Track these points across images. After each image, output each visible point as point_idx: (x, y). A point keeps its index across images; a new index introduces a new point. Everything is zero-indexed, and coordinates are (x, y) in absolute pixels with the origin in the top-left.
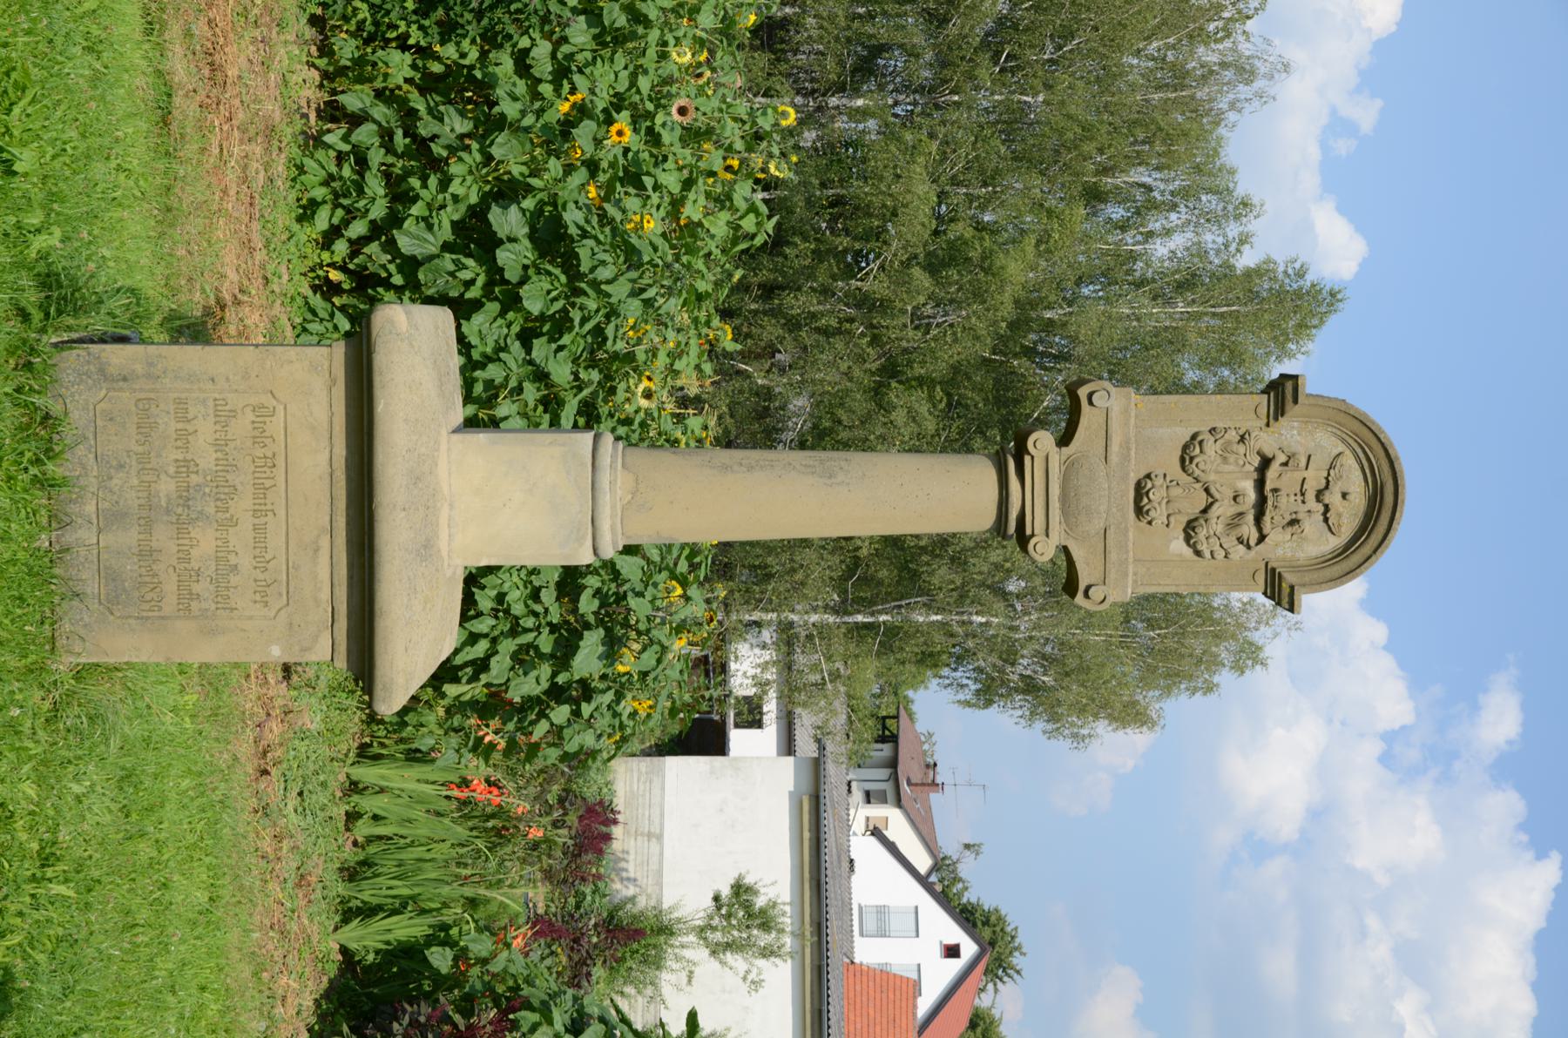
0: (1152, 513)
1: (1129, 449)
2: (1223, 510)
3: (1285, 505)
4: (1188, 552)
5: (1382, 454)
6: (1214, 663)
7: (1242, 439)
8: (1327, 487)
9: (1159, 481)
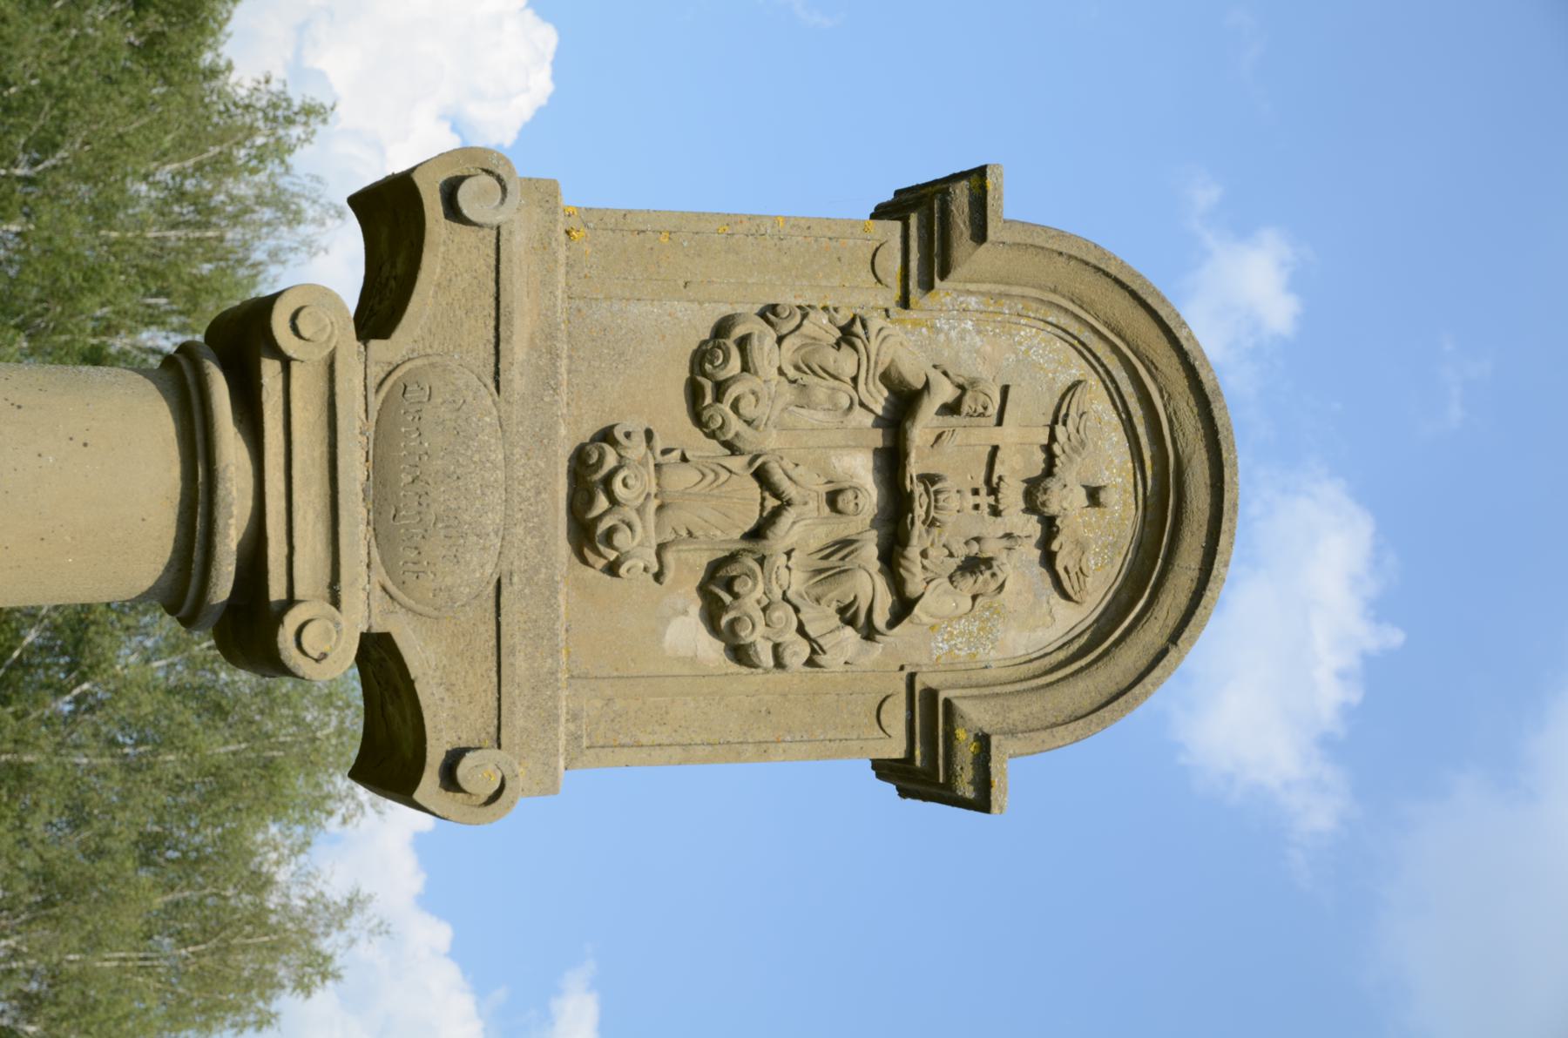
0: (621, 539)
1: (554, 356)
2: (803, 530)
3: (951, 522)
4: (712, 650)
5: (1180, 384)
6: (265, 984)
7: (847, 336)
8: (1049, 471)
9: (636, 450)
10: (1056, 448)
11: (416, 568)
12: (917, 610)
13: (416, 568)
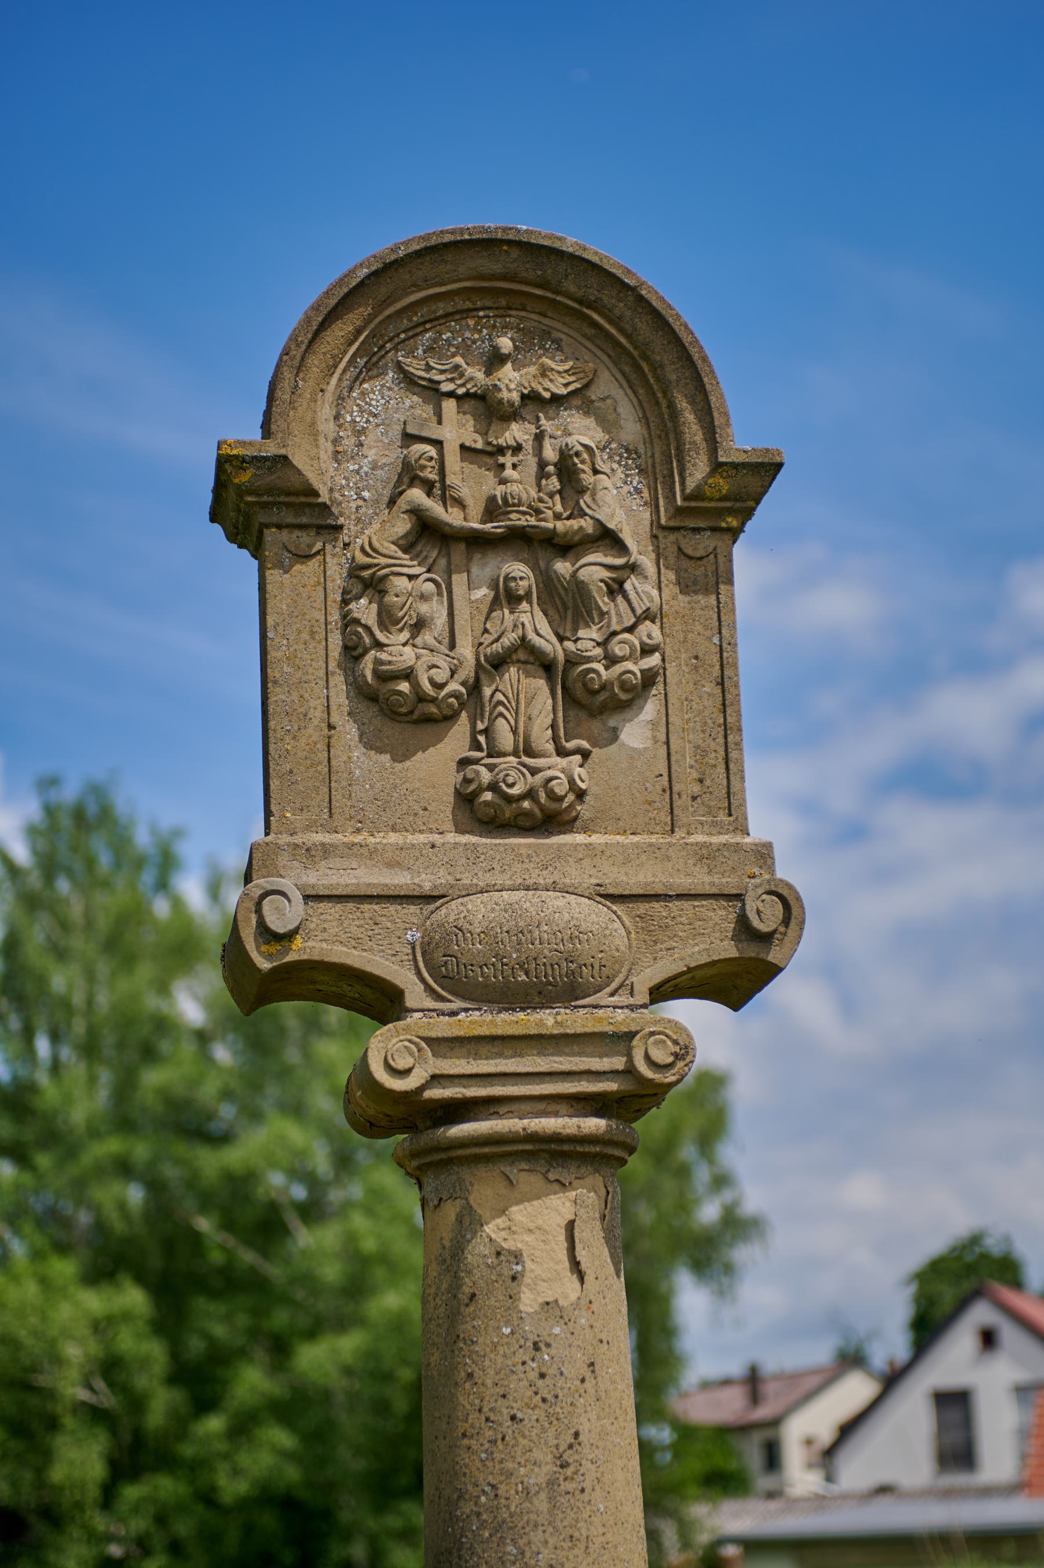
10: (461, 391)
11: (597, 967)
12: (611, 526)
13: (597, 967)
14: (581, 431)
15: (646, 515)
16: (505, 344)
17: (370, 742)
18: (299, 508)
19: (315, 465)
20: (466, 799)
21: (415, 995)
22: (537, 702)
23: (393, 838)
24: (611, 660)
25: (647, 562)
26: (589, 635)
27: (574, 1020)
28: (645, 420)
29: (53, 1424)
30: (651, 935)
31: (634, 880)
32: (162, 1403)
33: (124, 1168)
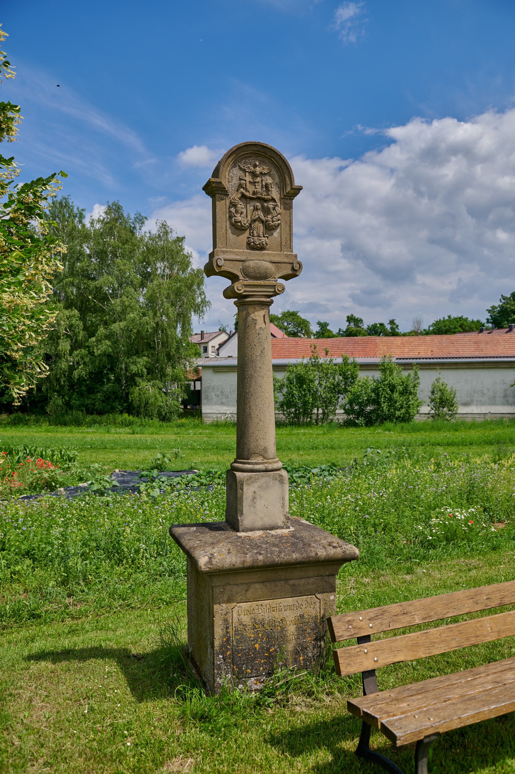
14: (269, 180)
15: (279, 196)
16: (257, 163)
17: (233, 233)
18: (222, 191)
19: (225, 184)
20: (248, 244)
21: (241, 277)
22: (261, 228)
23: (237, 250)
24: (273, 221)
25: (279, 204)
26: (270, 217)
27: (266, 282)
28: (279, 178)
29: (59, 338)
30: (278, 269)
31: (276, 259)
32: (82, 334)
33: (72, 284)
